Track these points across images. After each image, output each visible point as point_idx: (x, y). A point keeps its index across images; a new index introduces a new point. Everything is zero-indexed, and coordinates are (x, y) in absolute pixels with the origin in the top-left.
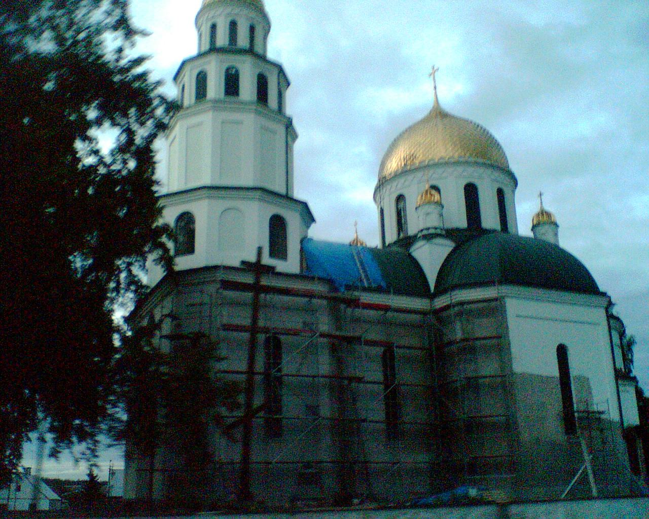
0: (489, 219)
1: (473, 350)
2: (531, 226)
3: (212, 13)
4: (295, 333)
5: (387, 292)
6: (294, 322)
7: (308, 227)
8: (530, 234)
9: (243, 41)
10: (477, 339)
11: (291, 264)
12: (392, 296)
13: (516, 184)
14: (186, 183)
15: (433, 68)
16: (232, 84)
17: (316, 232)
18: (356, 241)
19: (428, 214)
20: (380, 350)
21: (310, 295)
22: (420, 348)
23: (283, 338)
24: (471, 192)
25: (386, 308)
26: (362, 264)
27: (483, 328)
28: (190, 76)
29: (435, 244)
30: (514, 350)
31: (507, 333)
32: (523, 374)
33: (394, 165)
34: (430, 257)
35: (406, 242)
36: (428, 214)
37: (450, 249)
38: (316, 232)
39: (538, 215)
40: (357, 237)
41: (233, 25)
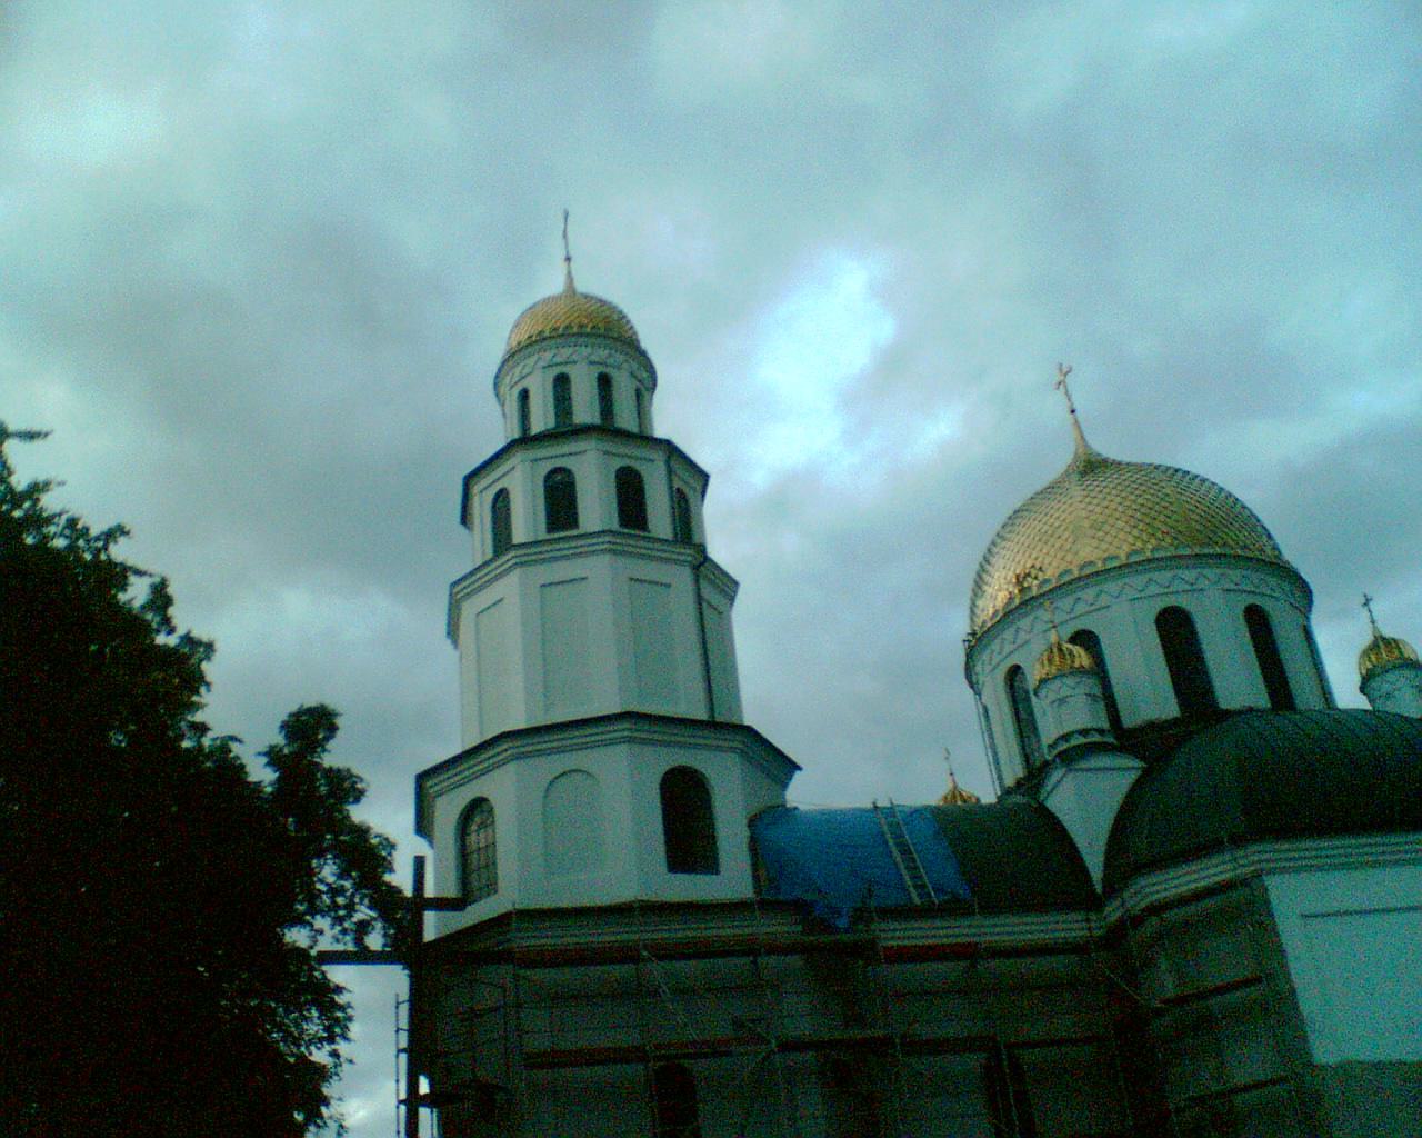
0: (1236, 681)
1: (1206, 1023)
2: (1357, 680)
3: (566, 352)
4: (716, 1050)
5: (967, 912)
6: (715, 1022)
7: (784, 786)
8: (1362, 703)
9: (585, 409)
10: (1220, 990)
11: (732, 879)
12: (978, 920)
13: (1306, 592)
14: (481, 733)
15: (1061, 370)
16: (560, 499)
17: (802, 794)
18: (955, 793)
19: (1062, 701)
20: (974, 1061)
21: (751, 948)
22: (1088, 1041)
23: (699, 1068)
24: (1176, 630)
25: (967, 952)
26: (905, 851)
27: (1222, 960)
28: (481, 504)
29: (1082, 770)
30: (1309, 1004)
31: (1284, 967)
32: (1346, 1070)
33: (998, 593)
34: (1087, 804)
35: (1035, 775)
36: (1062, 701)
37: (1133, 776)
38: (802, 794)
39: (1366, 654)
40: (955, 787)
41: (562, 382)
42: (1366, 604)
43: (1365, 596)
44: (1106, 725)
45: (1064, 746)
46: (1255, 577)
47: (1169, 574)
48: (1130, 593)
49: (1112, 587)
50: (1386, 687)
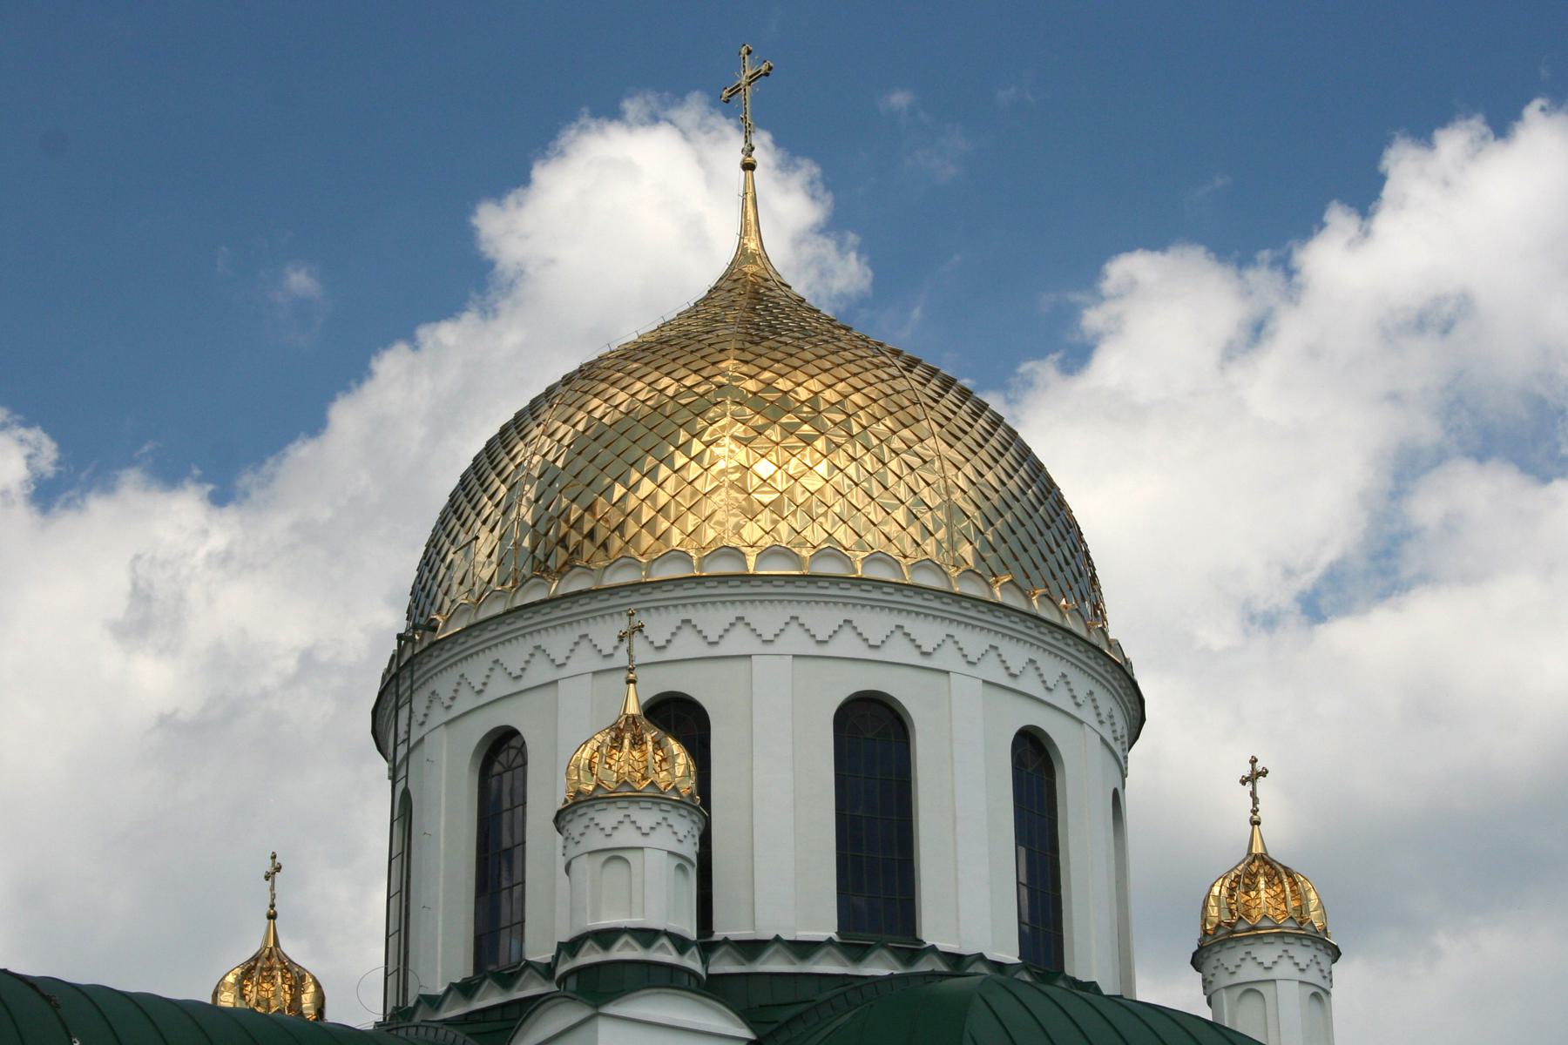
24: (872, 743)
42: (278, 869)
43: (1254, 761)
44: (690, 930)
45: (590, 956)
46: (1052, 668)
47: (836, 615)
48: (795, 641)
49: (767, 618)
50: (1249, 972)
